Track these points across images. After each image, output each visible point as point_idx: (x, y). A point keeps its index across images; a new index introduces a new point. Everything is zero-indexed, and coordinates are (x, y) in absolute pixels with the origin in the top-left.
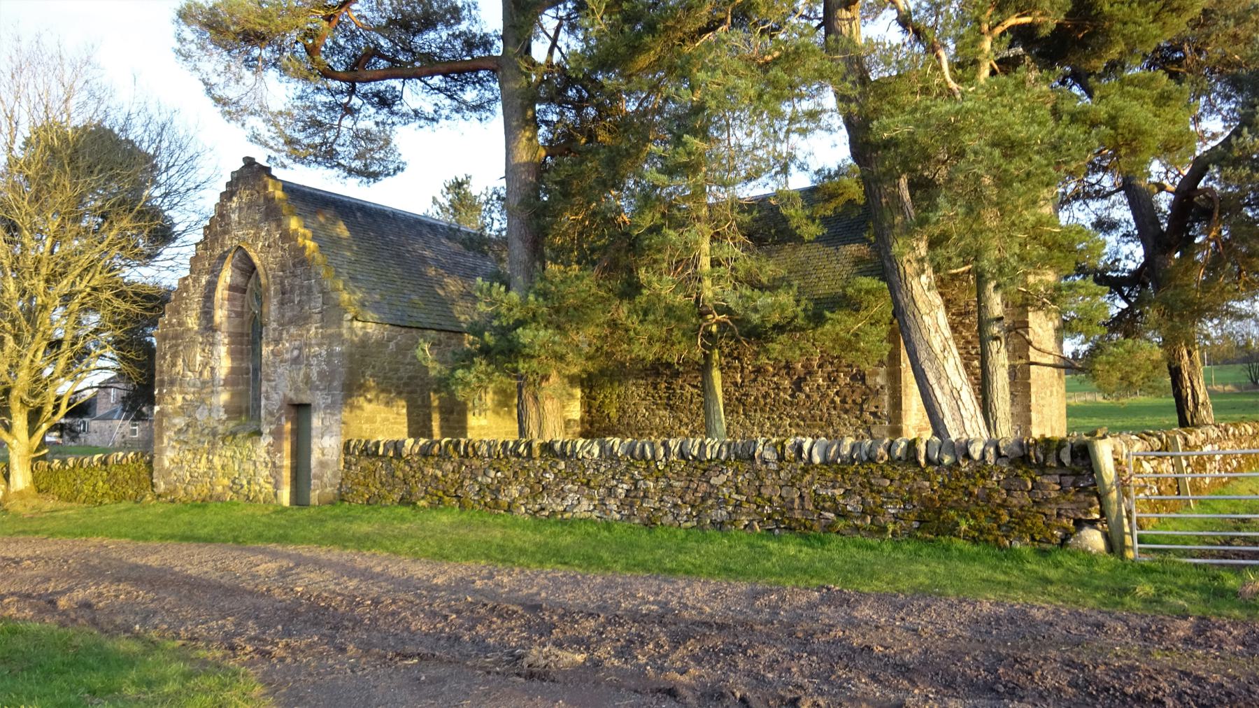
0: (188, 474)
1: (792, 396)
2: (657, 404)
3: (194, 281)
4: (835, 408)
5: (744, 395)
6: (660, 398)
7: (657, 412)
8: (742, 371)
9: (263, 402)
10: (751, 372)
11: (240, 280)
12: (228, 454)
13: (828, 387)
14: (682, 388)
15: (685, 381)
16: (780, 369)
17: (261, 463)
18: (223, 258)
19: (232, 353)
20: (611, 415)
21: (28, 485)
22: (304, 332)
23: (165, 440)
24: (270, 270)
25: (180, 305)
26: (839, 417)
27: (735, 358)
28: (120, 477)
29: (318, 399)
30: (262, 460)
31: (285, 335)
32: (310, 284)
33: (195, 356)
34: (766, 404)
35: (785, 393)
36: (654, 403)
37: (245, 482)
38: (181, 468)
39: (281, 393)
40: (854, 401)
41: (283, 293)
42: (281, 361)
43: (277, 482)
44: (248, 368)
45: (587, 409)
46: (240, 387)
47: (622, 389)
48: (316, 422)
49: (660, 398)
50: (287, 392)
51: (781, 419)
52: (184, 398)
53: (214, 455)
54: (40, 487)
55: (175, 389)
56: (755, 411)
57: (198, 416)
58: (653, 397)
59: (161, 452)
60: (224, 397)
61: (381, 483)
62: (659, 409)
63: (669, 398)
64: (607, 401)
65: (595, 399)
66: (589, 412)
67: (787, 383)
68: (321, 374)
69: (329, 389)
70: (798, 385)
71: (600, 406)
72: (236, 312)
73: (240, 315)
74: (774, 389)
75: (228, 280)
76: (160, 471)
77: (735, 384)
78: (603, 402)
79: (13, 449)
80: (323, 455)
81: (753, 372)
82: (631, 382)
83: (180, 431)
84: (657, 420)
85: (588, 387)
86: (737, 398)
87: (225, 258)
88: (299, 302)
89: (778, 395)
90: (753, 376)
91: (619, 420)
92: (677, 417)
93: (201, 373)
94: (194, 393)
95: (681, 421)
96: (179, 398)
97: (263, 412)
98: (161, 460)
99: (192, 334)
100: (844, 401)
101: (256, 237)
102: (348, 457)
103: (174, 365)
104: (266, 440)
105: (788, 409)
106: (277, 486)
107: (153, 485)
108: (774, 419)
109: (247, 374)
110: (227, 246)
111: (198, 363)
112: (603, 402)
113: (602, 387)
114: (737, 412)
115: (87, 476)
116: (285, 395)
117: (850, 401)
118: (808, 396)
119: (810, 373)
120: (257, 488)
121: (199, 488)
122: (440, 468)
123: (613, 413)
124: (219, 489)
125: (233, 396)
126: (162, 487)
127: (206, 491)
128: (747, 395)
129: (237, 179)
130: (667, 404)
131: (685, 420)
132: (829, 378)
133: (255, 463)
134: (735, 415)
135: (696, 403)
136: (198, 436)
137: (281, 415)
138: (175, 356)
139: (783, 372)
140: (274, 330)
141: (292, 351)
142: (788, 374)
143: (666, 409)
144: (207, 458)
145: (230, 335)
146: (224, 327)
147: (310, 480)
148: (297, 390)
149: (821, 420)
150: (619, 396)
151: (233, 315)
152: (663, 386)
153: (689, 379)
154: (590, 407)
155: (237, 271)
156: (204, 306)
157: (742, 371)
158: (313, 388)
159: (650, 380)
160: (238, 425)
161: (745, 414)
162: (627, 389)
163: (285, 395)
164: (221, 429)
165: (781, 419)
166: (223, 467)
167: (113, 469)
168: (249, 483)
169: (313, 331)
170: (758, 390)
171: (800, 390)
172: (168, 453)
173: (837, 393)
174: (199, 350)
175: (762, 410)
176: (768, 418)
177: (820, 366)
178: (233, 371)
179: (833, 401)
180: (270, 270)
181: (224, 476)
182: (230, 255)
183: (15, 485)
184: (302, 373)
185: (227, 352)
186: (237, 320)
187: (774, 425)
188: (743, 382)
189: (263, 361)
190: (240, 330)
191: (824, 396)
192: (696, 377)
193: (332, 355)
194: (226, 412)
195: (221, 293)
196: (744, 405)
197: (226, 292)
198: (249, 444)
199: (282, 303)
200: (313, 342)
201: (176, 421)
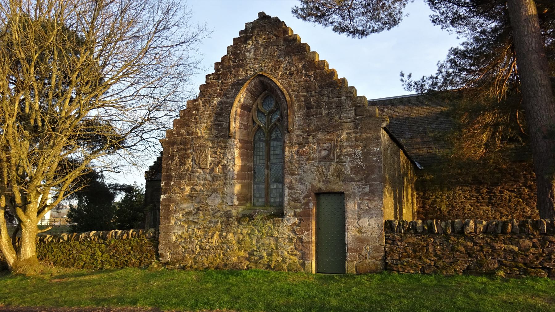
0: (198, 247)
2: (481, 202)
3: (204, 102)
6: (483, 198)
7: (480, 207)
9: (287, 192)
11: (249, 101)
12: (245, 231)
14: (501, 192)
15: (503, 188)
17: (284, 239)
18: (238, 85)
19: (242, 155)
20: (442, 209)
21: (34, 254)
22: (335, 138)
23: (173, 221)
24: (293, 91)
25: (189, 120)
28: (120, 249)
30: (285, 236)
31: (311, 139)
32: (341, 102)
33: (206, 157)
36: (478, 202)
37: (265, 254)
38: (191, 242)
39: (308, 184)
41: (308, 108)
42: (308, 160)
43: (304, 254)
44: (251, 167)
45: (421, 205)
46: (246, 181)
47: (451, 193)
48: (351, 206)
49: (483, 198)
50: (316, 183)
52: (192, 189)
53: (228, 232)
54: (41, 256)
55: (183, 182)
57: (209, 203)
58: (477, 198)
59: (168, 230)
60: (237, 188)
61: (436, 255)
62: (483, 206)
63: (490, 199)
64: (438, 200)
65: (428, 199)
66: (424, 207)
68: (356, 170)
71: (432, 203)
72: (244, 125)
73: (246, 127)
75: (242, 100)
76: (165, 244)
78: (435, 201)
79: (26, 226)
80: (360, 232)
82: (458, 188)
83: (189, 213)
84: (481, 212)
85: (422, 191)
87: (242, 85)
88: (327, 115)
91: (449, 212)
92: (498, 211)
93: (212, 170)
94: (204, 185)
95: (502, 213)
96: (188, 189)
98: (167, 235)
99: (202, 141)
101: (276, 67)
102: (391, 235)
103: (183, 164)
104: (291, 220)
106: (304, 257)
107: (158, 255)
109: (251, 171)
110: (241, 76)
111: (209, 162)
112: (435, 201)
113: (434, 191)
115: (84, 247)
116: (312, 186)
120: (280, 259)
121: (210, 258)
122: (517, 244)
123: (444, 207)
124: (235, 259)
125: (243, 187)
126: (168, 256)
127: (218, 260)
129: (253, 28)
130: (489, 203)
131: (505, 213)
135: (513, 202)
136: (209, 218)
137: (309, 201)
138: (183, 157)
140: (298, 136)
141: (320, 152)
143: (488, 206)
144: (220, 235)
145: (241, 141)
146: (237, 136)
147: (345, 253)
148: (327, 181)
150: (448, 197)
151: (242, 127)
152: (485, 191)
153: (506, 186)
154: (424, 204)
155: (249, 94)
156: (216, 120)
158: (347, 180)
159: (474, 187)
160: (245, 209)
162: (455, 193)
163: (312, 186)
164: (234, 212)
166: (239, 242)
167: (113, 242)
168: (270, 255)
169: (344, 136)
172: (176, 231)
174: (209, 152)
178: (243, 168)
180: (293, 91)
181: (240, 249)
182: (248, 82)
183: (26, 254)
184: (332, 168)
185: (239, 154)
186: (245, 131)
189: (286, 160)
190: (246, 138)
192: (512, 185)
193: (369, 154)
194: (238, 199)
195: (236, 108)
197: (239, 110)
198: (270, 224)
199: (307, 116)
200: (345, 144)
201: (185, 206)
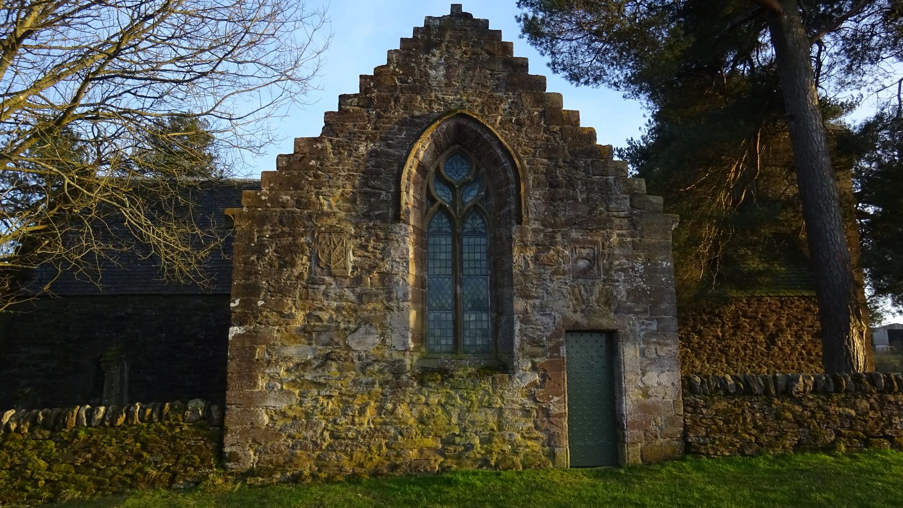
1: (768, 348)
4: (803, 359)
5: (726, 346)
8: (723, 327)
10: (730, 328)
12: (434, 400)
13: (796, 343)
16: (755, 326)
26: (807, 366)
27: (716, 315)
29: (631, 324)
32: (607, 182)
34: (746, 354)
35: (761, 346)
38: (310, 425)
40: (817, 354)
42: (555, 273)
50: (570, 314)
51: (760, 367)
56: (737, 360)
61: (756, 427)
67: (761, 338)
69: (653, 312)
70: (772, 339)
74: (751, 342)
77: (717, 337)
80: (646, 394)
81: (732, 328)
86: (719, 349)
89: (756, 347)
90: (731, 331)
97: (517, 340)
100: (809, 354)
105: (765, 359)
108: (754, 367)
114: (721, 361)
117: (814, 354)
118: (781, 349)
119: (782, 331)
121: (357, 454)
122: (853, 406)
128: (729, 347)
132: (796, 334)
133: (500, 411)
134: (719, 364)
139: (757, 329)
142: (762, 330)
149: (793, 368)
157: (723, 327)
161: (727, 363)
163: (565, 318)
165: (760, 367)
170: (738, 343)
171: (775, 344)
173: (803, 347)
174: (351, 245)
175: (743, 360)
176: (749, 367)
177: (788, 325)
179: (801, 354)
184: (597, 289)
187: (754, 372)
188: (723, 335)
191: (793, 349)
196: (727, 355)
198: (487, 385)
199: (551, 199)
